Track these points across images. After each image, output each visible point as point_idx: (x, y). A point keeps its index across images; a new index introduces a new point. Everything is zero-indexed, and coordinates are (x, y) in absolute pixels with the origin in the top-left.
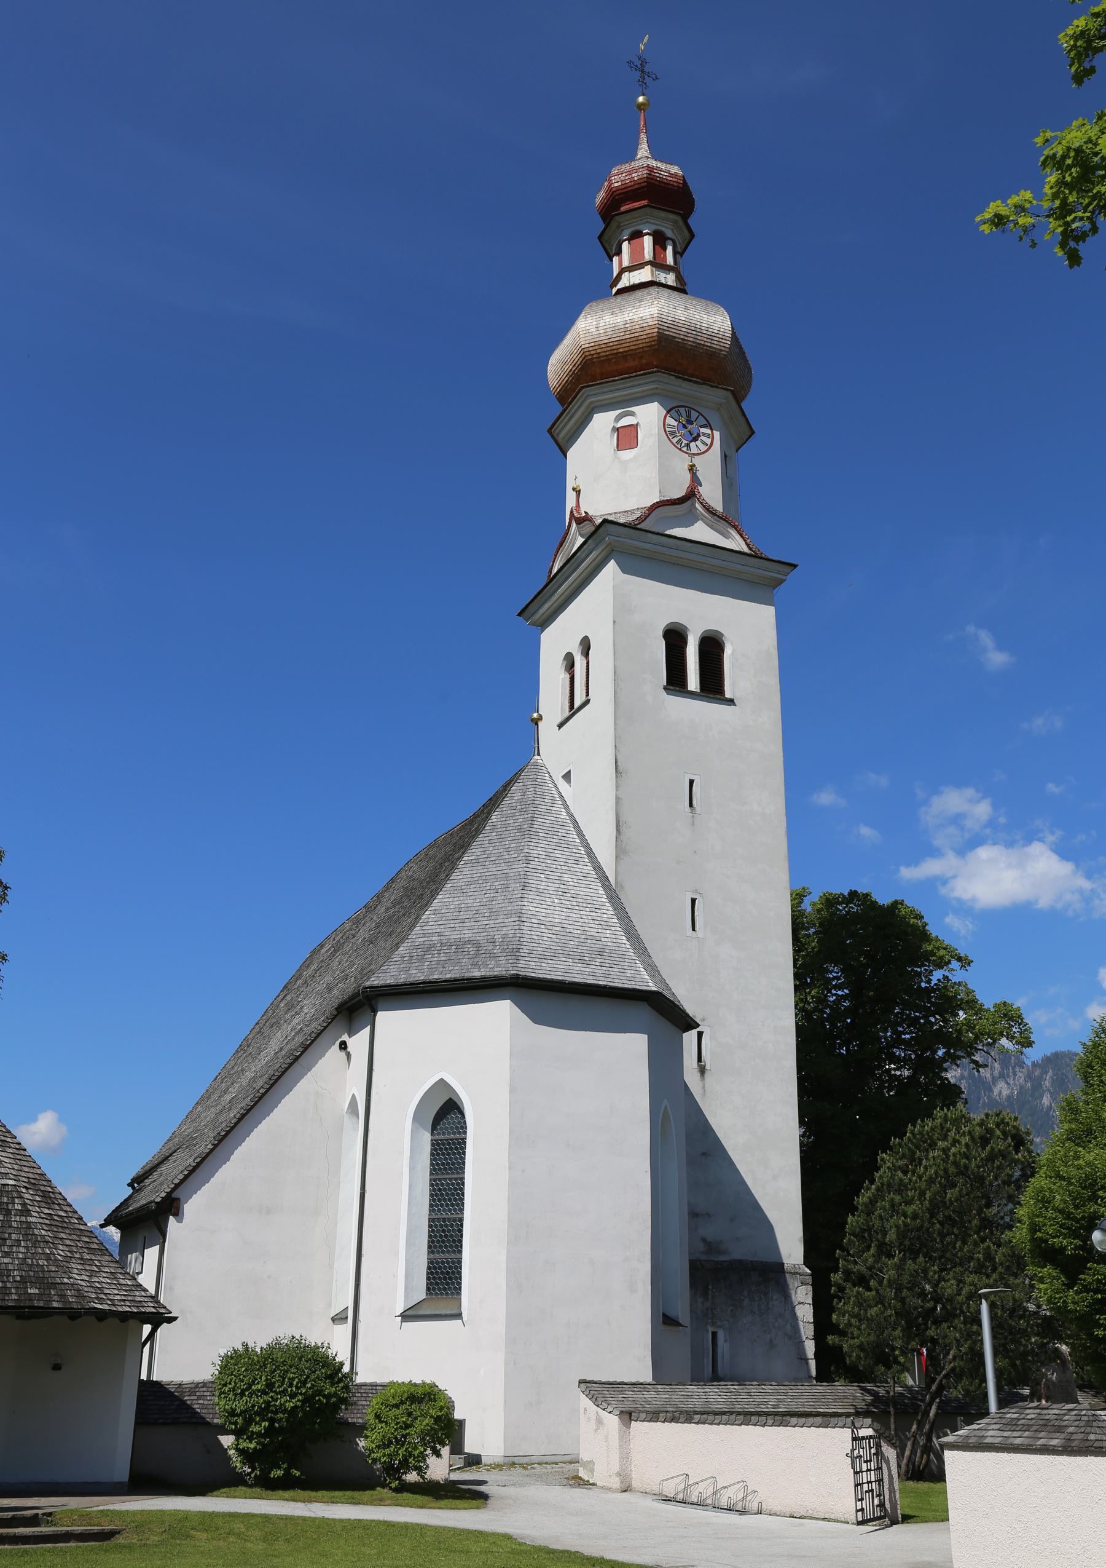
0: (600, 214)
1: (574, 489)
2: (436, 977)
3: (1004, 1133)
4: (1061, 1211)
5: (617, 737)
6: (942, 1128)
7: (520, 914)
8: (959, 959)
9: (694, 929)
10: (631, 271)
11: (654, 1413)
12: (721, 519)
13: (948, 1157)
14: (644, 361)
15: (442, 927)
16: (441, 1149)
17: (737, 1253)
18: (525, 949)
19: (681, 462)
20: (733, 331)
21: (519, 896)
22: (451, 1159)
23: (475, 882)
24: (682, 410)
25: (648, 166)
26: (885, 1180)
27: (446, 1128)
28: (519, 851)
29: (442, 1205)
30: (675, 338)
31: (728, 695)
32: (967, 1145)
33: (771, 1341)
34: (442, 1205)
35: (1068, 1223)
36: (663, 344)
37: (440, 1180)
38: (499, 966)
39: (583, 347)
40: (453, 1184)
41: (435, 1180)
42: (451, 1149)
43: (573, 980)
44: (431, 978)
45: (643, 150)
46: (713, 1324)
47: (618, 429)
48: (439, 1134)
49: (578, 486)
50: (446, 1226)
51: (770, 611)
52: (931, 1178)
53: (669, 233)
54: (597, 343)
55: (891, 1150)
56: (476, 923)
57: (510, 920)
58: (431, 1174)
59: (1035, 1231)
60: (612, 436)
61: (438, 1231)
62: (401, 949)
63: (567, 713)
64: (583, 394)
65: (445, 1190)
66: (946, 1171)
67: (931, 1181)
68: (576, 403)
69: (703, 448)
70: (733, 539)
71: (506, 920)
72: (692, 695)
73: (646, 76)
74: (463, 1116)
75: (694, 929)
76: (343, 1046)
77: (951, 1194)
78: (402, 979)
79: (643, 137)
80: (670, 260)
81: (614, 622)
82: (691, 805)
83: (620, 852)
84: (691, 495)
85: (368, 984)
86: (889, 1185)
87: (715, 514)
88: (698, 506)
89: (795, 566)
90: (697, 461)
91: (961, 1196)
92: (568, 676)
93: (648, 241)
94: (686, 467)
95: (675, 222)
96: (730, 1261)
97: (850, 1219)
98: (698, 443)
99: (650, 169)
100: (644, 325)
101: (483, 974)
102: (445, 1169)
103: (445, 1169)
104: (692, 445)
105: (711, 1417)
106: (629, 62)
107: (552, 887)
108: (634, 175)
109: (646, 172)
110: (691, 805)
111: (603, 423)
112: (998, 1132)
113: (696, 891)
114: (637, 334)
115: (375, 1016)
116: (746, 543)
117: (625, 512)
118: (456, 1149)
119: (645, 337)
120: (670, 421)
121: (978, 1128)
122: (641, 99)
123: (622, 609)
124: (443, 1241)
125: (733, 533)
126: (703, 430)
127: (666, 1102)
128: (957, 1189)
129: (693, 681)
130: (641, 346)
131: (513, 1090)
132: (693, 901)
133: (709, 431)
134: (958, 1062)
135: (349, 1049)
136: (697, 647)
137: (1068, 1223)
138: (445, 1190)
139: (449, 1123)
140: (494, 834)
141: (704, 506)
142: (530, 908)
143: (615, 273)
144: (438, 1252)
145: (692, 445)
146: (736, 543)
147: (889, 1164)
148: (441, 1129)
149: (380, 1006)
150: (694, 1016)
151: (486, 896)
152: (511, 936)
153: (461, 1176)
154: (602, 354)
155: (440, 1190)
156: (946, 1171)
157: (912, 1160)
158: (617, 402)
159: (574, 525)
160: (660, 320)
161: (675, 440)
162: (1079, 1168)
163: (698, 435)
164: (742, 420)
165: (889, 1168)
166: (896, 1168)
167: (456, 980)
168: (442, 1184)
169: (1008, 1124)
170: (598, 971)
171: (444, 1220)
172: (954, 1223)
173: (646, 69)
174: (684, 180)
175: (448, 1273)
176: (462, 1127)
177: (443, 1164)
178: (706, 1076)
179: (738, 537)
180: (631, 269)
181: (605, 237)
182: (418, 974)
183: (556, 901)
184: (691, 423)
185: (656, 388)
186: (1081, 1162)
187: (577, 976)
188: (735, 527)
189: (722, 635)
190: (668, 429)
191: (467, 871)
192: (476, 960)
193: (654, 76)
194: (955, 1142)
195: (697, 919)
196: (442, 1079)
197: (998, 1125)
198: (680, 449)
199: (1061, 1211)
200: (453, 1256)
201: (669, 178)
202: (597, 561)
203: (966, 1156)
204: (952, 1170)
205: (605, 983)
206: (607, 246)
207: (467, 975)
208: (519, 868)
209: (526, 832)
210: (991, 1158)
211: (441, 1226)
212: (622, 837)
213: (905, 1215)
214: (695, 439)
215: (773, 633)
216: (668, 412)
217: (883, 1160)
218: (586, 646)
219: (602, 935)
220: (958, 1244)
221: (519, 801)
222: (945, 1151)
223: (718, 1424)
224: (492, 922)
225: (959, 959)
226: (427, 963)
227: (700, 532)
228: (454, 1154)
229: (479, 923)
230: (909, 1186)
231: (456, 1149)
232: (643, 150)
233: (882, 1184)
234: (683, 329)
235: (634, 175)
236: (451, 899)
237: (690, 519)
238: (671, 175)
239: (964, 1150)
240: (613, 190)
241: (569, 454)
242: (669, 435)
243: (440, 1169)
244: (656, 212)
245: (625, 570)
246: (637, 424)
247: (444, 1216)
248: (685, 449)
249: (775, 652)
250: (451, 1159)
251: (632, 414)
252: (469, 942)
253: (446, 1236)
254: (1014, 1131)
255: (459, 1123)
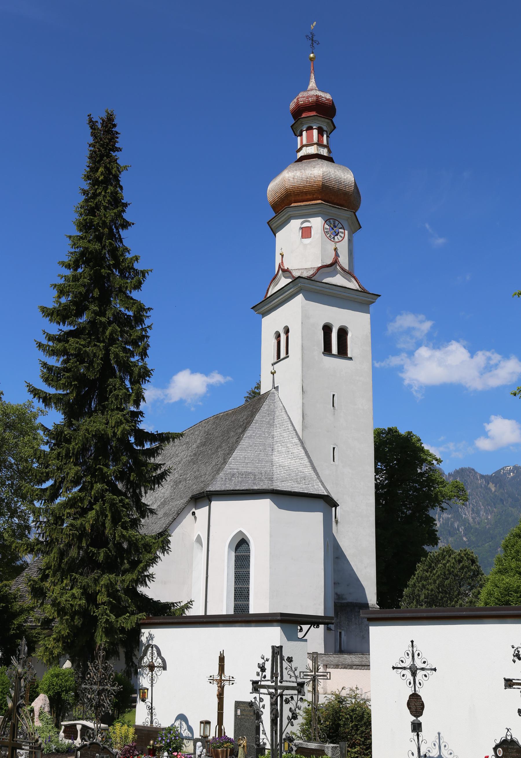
0: (292, 114)
1: (280, 254)
2: (238, 488)
3: (467, 558)
4: (497, 598)
5: (303, 376)
6: (442, 555)
7: (272, 462)
8: (437, 460)
9: (334, 461)
10: (307, 147)
11: (337, 665)
12: (349, 274)
13: (445, 567)
14: (315, 196)
15: (238, 465)
16: (239, 559)
17: (350, 599)
18: (275, 477)
19: (331, 246)
20: (355, 182)
21: (271, 454)
22: (243, 563)
23: (251, 446)
24: (331, 221)
25: (316, 95)
26: (420, 575)
27: (241, 550)
28: (269, 433)
29: (240, 582)
30: (329, 186)
31: (349, 356)
32: (453, 563)
33: (363, 636)
34: (240, 582)
35: (499, 603)
36: (324, 189)
37: (239, 571)
38: (265, 485)
39: (287, 187)
40: (245, 573)
41: (237, 572)
42: (243, 559)
43: (295, 491)
44: (236, 488)
45: (312, 84)
46: (340, 628)
47: (302, 228)
48: (238, 553)
49: (283, 253)
50: (242, 590)
51: (368, 316)
52: (439, 575)
53: (325, 128)
54: (293, 186)
55: (421, 562)
56: (253, 465)
57: (267, 464)
58: (235, 569)
59: (487, 605)
60: (299, 232)
61: (238, 592)
62: (220, 475)
63: (276, 360)
64: (287, 210)
65: (241, 576)
66: (444, 573)
67: (439, 576)
68: (283, 213)
69: (340, 239)
70: (353, 282)
71: (266, 464)
72: (334, 356)
73: (314, 43)
74: (249, 546)
75: (334, 461)
76: (194, 513)
77: (447, 582)
78: (223, 488)
79: (312, 75)
80: (325, 142)
81: (302, 323)
82: (333, 406)
83: (304, 427)
84: (335, 262)
85: (208, 490)
86: (421, 577)
87: (345, 271)
88: (338, 267)
89: (380, 296)
90: (338, 245)
91: (451, 583)
92: (276, 341)
93: (315, 132)
94: (333, 248)
95: (328, 123)
96: (347, 603)
97: (405, 590)
98: (338, 236)
99: (317, 96)
100: (316, 180)
101: (258, 488)
102: (241, 567)
103: (241, 567)
104: (336, 237)
105: (360, 667)
106: (307, 36)
107: (284, 449)
108: (309, 99)
109: (315, 98)
110: (333, 406)
111: (295, 224)
112: (465, 558)
113: (335, 444)
114: (312, 184)
115: (211, 503)
116: (359, 285)
117: (306, 269)
118: (246, 559)
119: (316, 185)
120: (326, 226)
121: (458, 556)
122: (312, 55)
123: (305, 317)
124: (241, 597)
125: (353, 280)
126: (340, 230)
127: (328, 539)
128: (449, 580)
129: (335, 350)
130: (314, 189)
131: (271, 536)
132: (334, 448)
133: (343, 231)
134: (434, 508)
135: (196, 515)
136: (337, 332)
137: (499, 603)
138: (241, 576)
139: (242, 548)
140: (257, 424)
141: (342, 269)
142: (275, 459)
143: (299, 147)
144: (239, 601)
145: (336, 237)
146: (353, 285)
147: (421, 569)
148: (239, 551)
149: (213, 499)
150: (337, 500)
151: (256, 453)
152: (269, 471)
153: (248, 570)
154: (295, 192)
155: (239, 576)
156: (444, 573)
157: (430, 567)
158: (283, 223)
159: (280, 272)
160: (323, 178)
161: (328, 236)
162: (504, 584)
163: (339, 233)
164: (357, 223)
165: (421, 570)
166: (424, 570)
167: (247, 490)
168: (240, 573)
169: (469, 555)
170: (304, 486)
171: (241, 588)
172: (446, 593)
173: (314, 39)
174: (333, 102)
175: (243, 609)
176: (248, 550)
177: (240, 565)
178: (338, 524)
179: (355, 282)
180: (307, 146)
181: (294, 127)
182: (230, 487)
183: (286, 455)
184: (335, 227)
185: (320, 211)
186: (504, 582)
187: (296, 489)
188: (354, 277)
189: (347, 328)
190: (325, 230)
191: (247, 440)
192: (255, 481)
193: (317, 42)
194: (448, 561)
195: (335, 456)
196: (240, 531)
197: (465, 555)
198: (330, 240)
199: (497, 598)
200: (245, 603)
201: (326, 101)
202: (293, 293)
203: (453, 567)
204: (447, 572)
205: (307, 492)
206: (294, 130)
207: (252, 488)
208: (270, 441)
209: (271, 425)
210: (462, 568)
211: (240, 590)
212: (305, 421)
213: (428, 589)
214: (337, 235)
215: (369, 326)
216: (325, 222)
217: (418, 566)
218: (287, 331)
219: (304, 470)
220: (449, 602)
221: (267, 410)
222: (445, 565)
223: (363, 670)
224: (260, 465)
225: (437, 460)
226: (233, 482)
227: (338, 280)
228: (245, 561)
229: (254, 465)
230: (429, 578)
231: (246, 559)
232: (312, 84)
233: (418, 577)
234: (333, 182)
235: (309, 99)
236: (241, 453)
237: (333, 275)
238: (327, 99)
239: (452, 565)
240: (300, 105)
241: (277, 235)
242: (326, 233)
243: (239, 567)
244: (320, 119)
245: (307, 299)
246: (311, 227)
247: (241, 586)
248: (332, 240)
249: (370, 335)
250: (243, 563)
251: (309, 221)
252: (251, 473)
253: (242, 594)
254: (471, 558)
255: (247, 548)
